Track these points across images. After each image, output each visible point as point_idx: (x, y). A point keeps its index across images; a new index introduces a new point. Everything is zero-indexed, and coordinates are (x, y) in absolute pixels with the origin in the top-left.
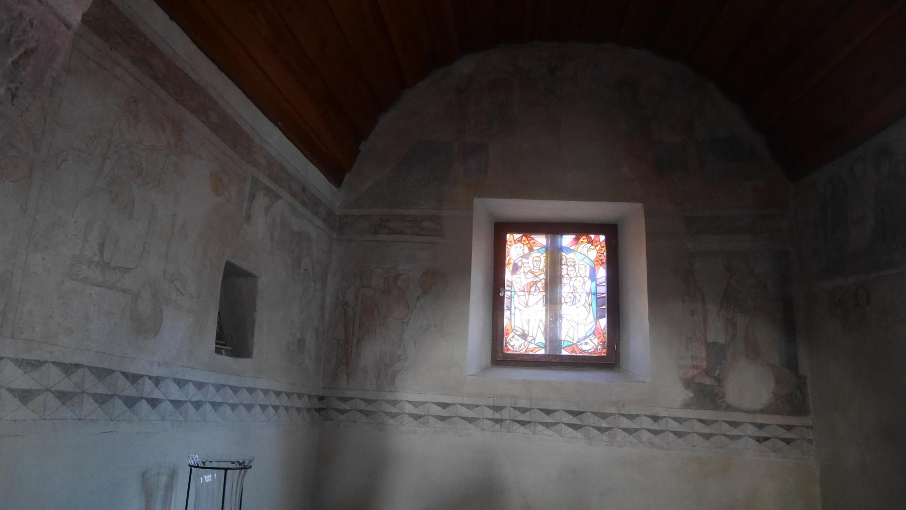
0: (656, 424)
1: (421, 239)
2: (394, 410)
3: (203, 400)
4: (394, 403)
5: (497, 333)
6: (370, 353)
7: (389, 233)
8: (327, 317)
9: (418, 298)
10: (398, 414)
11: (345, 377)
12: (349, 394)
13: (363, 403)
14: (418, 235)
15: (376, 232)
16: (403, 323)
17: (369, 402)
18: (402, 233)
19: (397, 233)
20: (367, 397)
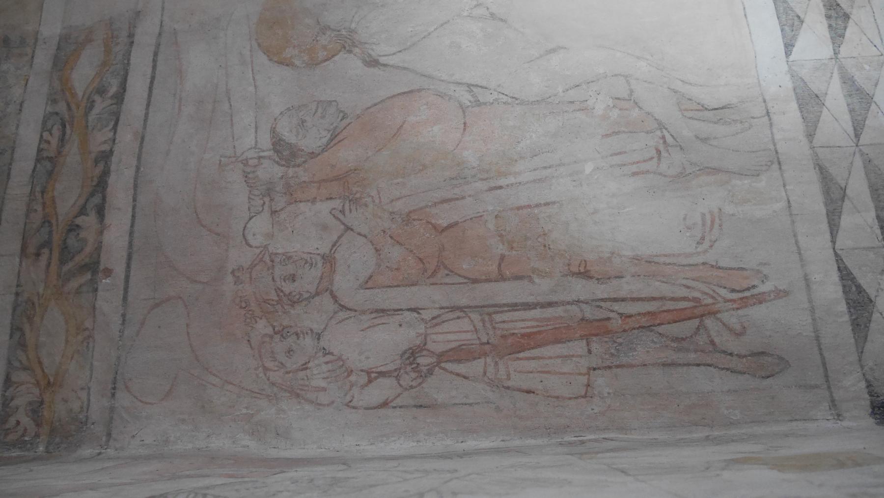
0: (808, 20)
1: (137, 86)
2: (836, 98)
3: (866, 402)
4: (809, 101)
5: (624, 99)
6: (625, 218)
7: (101, 211)
8: (517, 442)
9: (372, 63)
10: (847, 80)
11: (757, 313)
12: (830, 290)
13: (846, 221)
14: (120, 97)
15: (93, 267)
16: (478, 103)
17: (835, 200)
18: (106, 157)
19: (106, 173)
20: (819, 207)
